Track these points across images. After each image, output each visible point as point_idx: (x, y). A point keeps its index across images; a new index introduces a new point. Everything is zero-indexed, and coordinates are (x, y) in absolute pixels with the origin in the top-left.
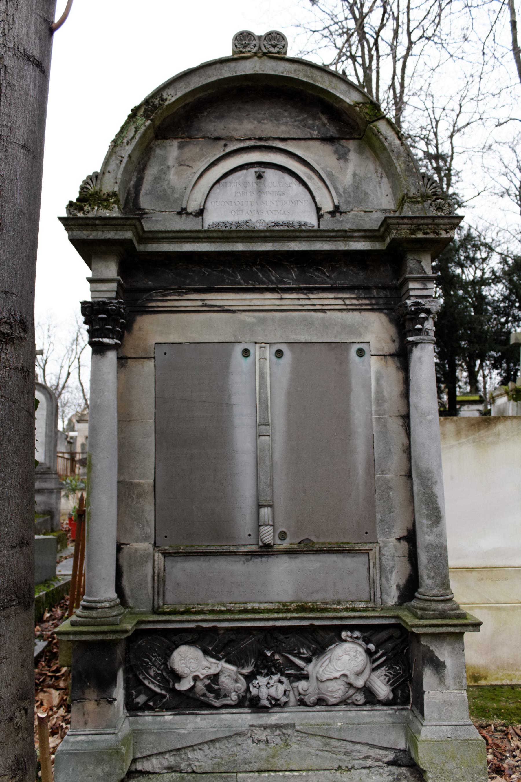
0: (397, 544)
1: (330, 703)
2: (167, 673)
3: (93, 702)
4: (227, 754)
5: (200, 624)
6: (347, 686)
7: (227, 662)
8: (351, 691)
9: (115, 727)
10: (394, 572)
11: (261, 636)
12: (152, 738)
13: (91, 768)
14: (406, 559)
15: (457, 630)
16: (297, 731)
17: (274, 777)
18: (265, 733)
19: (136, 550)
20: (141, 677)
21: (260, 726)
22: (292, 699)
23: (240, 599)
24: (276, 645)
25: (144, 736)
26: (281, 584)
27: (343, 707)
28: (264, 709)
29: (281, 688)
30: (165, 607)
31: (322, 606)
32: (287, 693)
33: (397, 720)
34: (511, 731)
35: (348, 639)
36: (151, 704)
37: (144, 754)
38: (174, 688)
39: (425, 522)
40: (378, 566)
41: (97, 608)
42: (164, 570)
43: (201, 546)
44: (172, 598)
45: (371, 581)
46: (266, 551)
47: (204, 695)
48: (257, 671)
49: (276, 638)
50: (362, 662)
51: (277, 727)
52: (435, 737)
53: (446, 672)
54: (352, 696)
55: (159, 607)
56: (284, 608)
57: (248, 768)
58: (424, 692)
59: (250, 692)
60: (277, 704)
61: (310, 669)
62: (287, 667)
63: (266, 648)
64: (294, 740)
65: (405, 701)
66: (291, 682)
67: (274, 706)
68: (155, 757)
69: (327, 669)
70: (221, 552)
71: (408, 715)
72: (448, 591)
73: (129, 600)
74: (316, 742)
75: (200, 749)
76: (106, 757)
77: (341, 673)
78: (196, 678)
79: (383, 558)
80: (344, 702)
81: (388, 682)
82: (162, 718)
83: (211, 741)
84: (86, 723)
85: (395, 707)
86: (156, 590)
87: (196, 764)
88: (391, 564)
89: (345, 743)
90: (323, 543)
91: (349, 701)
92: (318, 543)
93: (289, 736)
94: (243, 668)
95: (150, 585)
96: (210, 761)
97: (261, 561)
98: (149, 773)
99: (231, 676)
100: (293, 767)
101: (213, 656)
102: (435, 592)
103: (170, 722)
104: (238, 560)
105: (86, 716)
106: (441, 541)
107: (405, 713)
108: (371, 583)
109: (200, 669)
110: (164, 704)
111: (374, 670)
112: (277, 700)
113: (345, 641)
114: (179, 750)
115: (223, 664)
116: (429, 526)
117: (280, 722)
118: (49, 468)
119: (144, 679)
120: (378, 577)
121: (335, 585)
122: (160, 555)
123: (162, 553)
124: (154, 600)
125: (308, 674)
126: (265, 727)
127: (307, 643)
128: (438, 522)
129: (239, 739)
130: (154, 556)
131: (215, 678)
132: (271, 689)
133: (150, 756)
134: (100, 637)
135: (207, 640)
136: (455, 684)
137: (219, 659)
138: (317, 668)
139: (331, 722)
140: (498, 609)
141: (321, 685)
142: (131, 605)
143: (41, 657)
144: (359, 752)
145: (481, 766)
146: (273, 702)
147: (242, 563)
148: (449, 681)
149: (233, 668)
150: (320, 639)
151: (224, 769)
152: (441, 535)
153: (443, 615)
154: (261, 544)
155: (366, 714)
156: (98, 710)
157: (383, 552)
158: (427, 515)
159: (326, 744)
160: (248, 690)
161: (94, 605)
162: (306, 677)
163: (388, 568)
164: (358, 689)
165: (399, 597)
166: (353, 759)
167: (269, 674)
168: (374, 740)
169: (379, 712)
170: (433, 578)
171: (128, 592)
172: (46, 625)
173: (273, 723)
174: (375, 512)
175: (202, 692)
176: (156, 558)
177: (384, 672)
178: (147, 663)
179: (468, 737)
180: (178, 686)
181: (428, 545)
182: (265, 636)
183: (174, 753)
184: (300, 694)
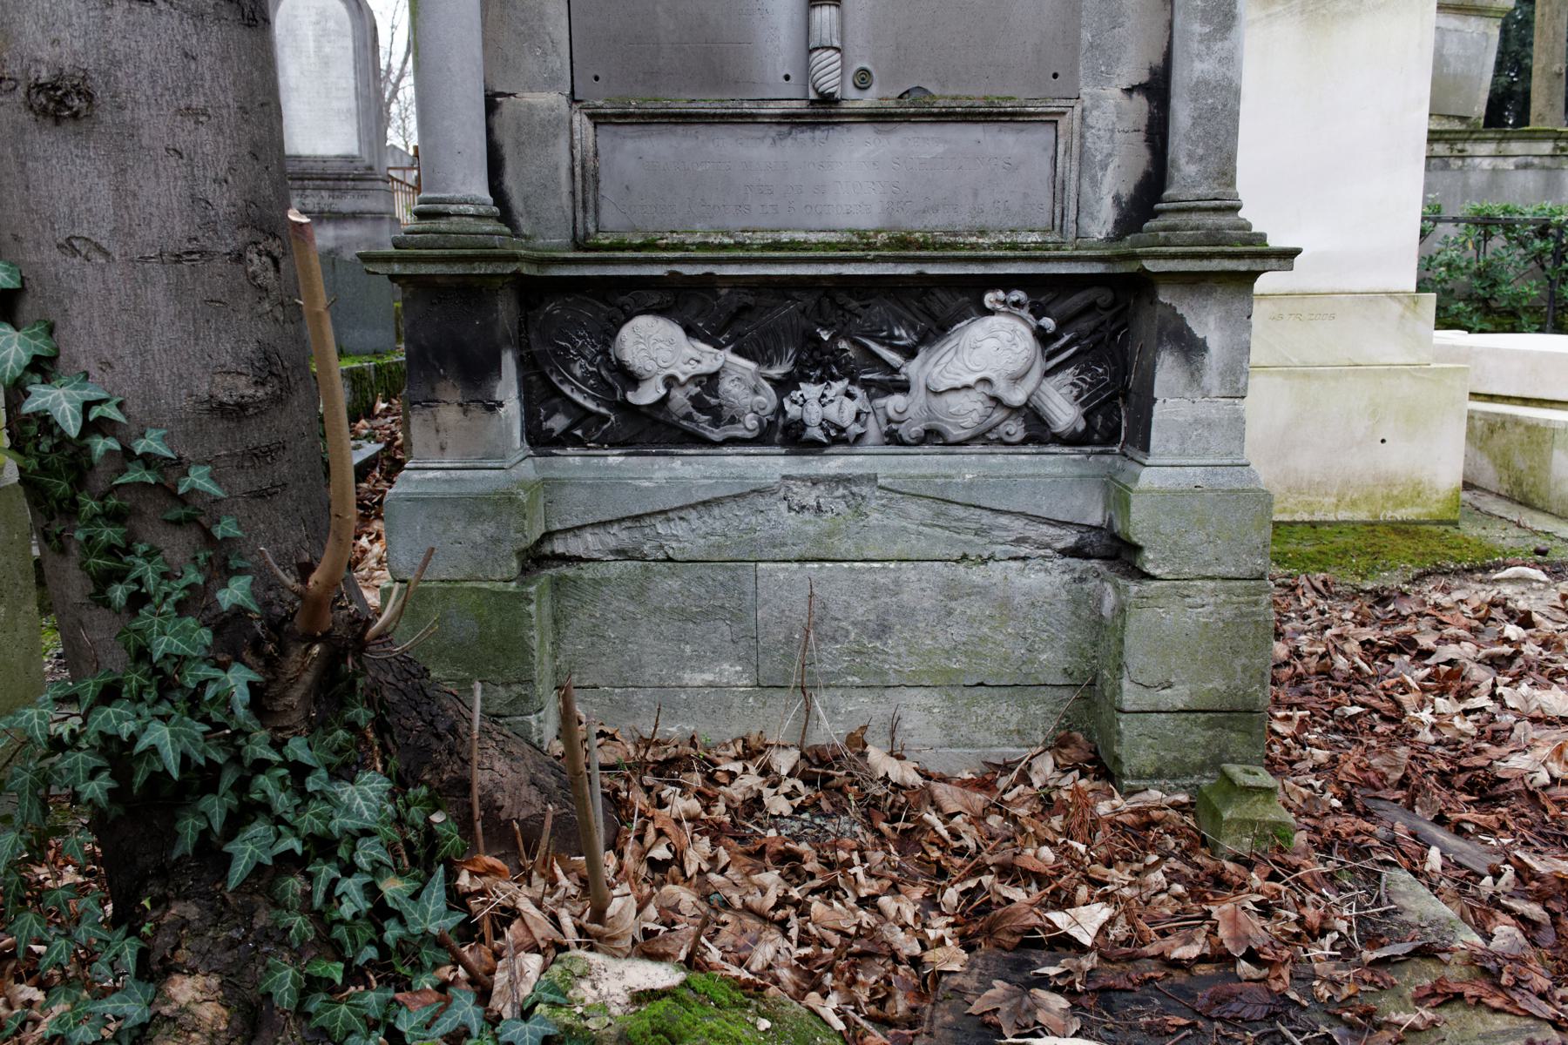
0: (1124, 101)
1: (951, 439)
2: (608, 370)
3: (455, 407)
4: (737, 528)
5: (677, 268)
6: (990, 404)
7: (734, 351)
8: (998, 415)
9: (503, 457)
10: (1111, 167)
11: (809, 301)
12: (583, 494)
13: (458, 527)
14: (1142, 136)
15: (1242, 266)
16: (881, 488)
17: (830, 569)
18: (815, 493)
19: (530, 107)
20: (554, 379)
21: (803, 479)
22: (873, 430)
23: (774, 224)
24: (841, 317)
25: (567, 491)
26: (853, 189)
27: (978, 448)
28: (815, 447)
29: (851, 407)
30: (600, 236)
31: (945, 239)
32: (863, 417)
33: (1090, 472)
34: (1303, 581)
35: (999, 306)
36: (579, 432)
37: (568, 525)
38: (626, 400)
39: (1197, 28)
40: (1075, 150)
41: (448, 215)
42: (596, 155)
43: (676, 101)
44: (614, 220)
45: (1058, 187)
46: (823, 112)
47: (688, 417)
48: (801, 372)
49: (841, 307)
50: (1025, 354)
51: (840, 480)
52: (1169, 484)
53: (1206, 361)
54: (998, 425)
55: (587, 235)
56: (861, 245)
57: (778, 553)
58: (1155, 400)
59: (785, 413)
60: (838, 438)
61: (912, 370)
62: (865, 366)
63: (820, 325)
64: (874, 504)
65: (1111, 437)
66: (871, 398)
67: (835, 441)
68: (589, 530)
69: (950, 368)
70: (723, 115)
71: (1114, 462)
72: (1230, 190)
73: (522, 221)
74: (917, 510)
75: (681, 518)
76: (487, 509)
77: (979, 375)
78: (671, 381)
79: (1088, 135)
80: (982, 438)
81: (1077, 398)
82: (602, 460)
83: (704, 503)
84: (442, 449)
85: (1088, 449)
86: (579, 197)
87: (674, 545)
88: (1107, 147)
89: (978, 512)
90: (955, 98)
91: (992, 436)
92: (942, 97)
93: (863, 498)
94: (770, 367)
95: (565, 189)
96: (702, 541)
97: (813, 139)
98: (579, 559)
99: (745, 383)
100: (871, 556)
101: (706, 340)
102: (1202, 191)
103: (618, 467)
104: (760, 134)
105: (442, 435)
106: (1229, 74)
107: (1108, 459)
108: (1058, 188)
109: (679, 363)
110: (605, 433)
111: (1048, 373)
112: (842, 430)
113: (991, 312)
114: (638, 518)
115: (727, 356)
116: (1207, 39)
117: (845, 471)
118: (370, 168)
119: (561, 382)
120: (1074, 176)
121: (976, 195)
122: (585, 119)
123: (590, 116)
124: (575, 219)
125: (907, 381)
126: (815, 481)
127: (911, 317)
128: (1229, 28)
129: (761, 502)
130: (571, 122)
131: (710, 381)
132: (829, 406)
133: (580, 528)
134: (458, 269)
135: (694, 302)
136: (1223, 385)
137: (720, 347)
138: (928, 368)
139: (953, 472)
140: (1306, 375)
141: (934, 401)
142: (526, 231)
143: (374, 467)
144: (1005, 528)
145: (1257, 540)
146: (833, 433)
147: (769, 141)
148: (1211, 379)
149: (752, 365)
150: (936, 308)
151: (732, 555)
152: (1230, 60)
153: (1215, 236)
154: (813, 96)
155: (1026, 462)
156: (466, 423)
157: (1089, 120)
158: (1203, 11)
159: (938, 515)
160: (781, 410)
161: (441, 207)
162: (904, 388)
163: (1099, 158)
164: (1014, 410)
165: (1117, 223)
166: (991, 543)
167: (826, 378)
168: (1040, 507)
169: (1052, 458)
170: (1201, 158)
171: (517, 203)
172: (381, 421)
173: (832, 472)
174: (1080, 26)
175: (684, 411)
176: (576, 125)
177: (1071, 379)
178: (566, 350)
179: (1237, 486)
180: (631, 397)
181: (1197, 83)
182: (819, 303)
183: (629, 524)
184: (889, 421)
